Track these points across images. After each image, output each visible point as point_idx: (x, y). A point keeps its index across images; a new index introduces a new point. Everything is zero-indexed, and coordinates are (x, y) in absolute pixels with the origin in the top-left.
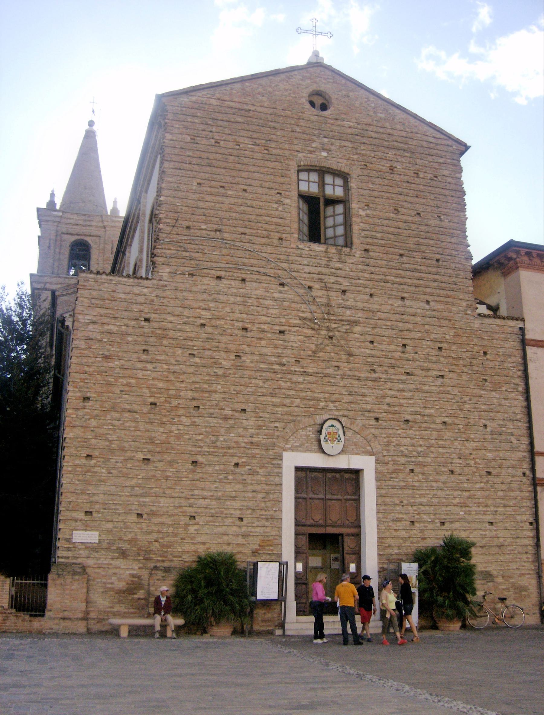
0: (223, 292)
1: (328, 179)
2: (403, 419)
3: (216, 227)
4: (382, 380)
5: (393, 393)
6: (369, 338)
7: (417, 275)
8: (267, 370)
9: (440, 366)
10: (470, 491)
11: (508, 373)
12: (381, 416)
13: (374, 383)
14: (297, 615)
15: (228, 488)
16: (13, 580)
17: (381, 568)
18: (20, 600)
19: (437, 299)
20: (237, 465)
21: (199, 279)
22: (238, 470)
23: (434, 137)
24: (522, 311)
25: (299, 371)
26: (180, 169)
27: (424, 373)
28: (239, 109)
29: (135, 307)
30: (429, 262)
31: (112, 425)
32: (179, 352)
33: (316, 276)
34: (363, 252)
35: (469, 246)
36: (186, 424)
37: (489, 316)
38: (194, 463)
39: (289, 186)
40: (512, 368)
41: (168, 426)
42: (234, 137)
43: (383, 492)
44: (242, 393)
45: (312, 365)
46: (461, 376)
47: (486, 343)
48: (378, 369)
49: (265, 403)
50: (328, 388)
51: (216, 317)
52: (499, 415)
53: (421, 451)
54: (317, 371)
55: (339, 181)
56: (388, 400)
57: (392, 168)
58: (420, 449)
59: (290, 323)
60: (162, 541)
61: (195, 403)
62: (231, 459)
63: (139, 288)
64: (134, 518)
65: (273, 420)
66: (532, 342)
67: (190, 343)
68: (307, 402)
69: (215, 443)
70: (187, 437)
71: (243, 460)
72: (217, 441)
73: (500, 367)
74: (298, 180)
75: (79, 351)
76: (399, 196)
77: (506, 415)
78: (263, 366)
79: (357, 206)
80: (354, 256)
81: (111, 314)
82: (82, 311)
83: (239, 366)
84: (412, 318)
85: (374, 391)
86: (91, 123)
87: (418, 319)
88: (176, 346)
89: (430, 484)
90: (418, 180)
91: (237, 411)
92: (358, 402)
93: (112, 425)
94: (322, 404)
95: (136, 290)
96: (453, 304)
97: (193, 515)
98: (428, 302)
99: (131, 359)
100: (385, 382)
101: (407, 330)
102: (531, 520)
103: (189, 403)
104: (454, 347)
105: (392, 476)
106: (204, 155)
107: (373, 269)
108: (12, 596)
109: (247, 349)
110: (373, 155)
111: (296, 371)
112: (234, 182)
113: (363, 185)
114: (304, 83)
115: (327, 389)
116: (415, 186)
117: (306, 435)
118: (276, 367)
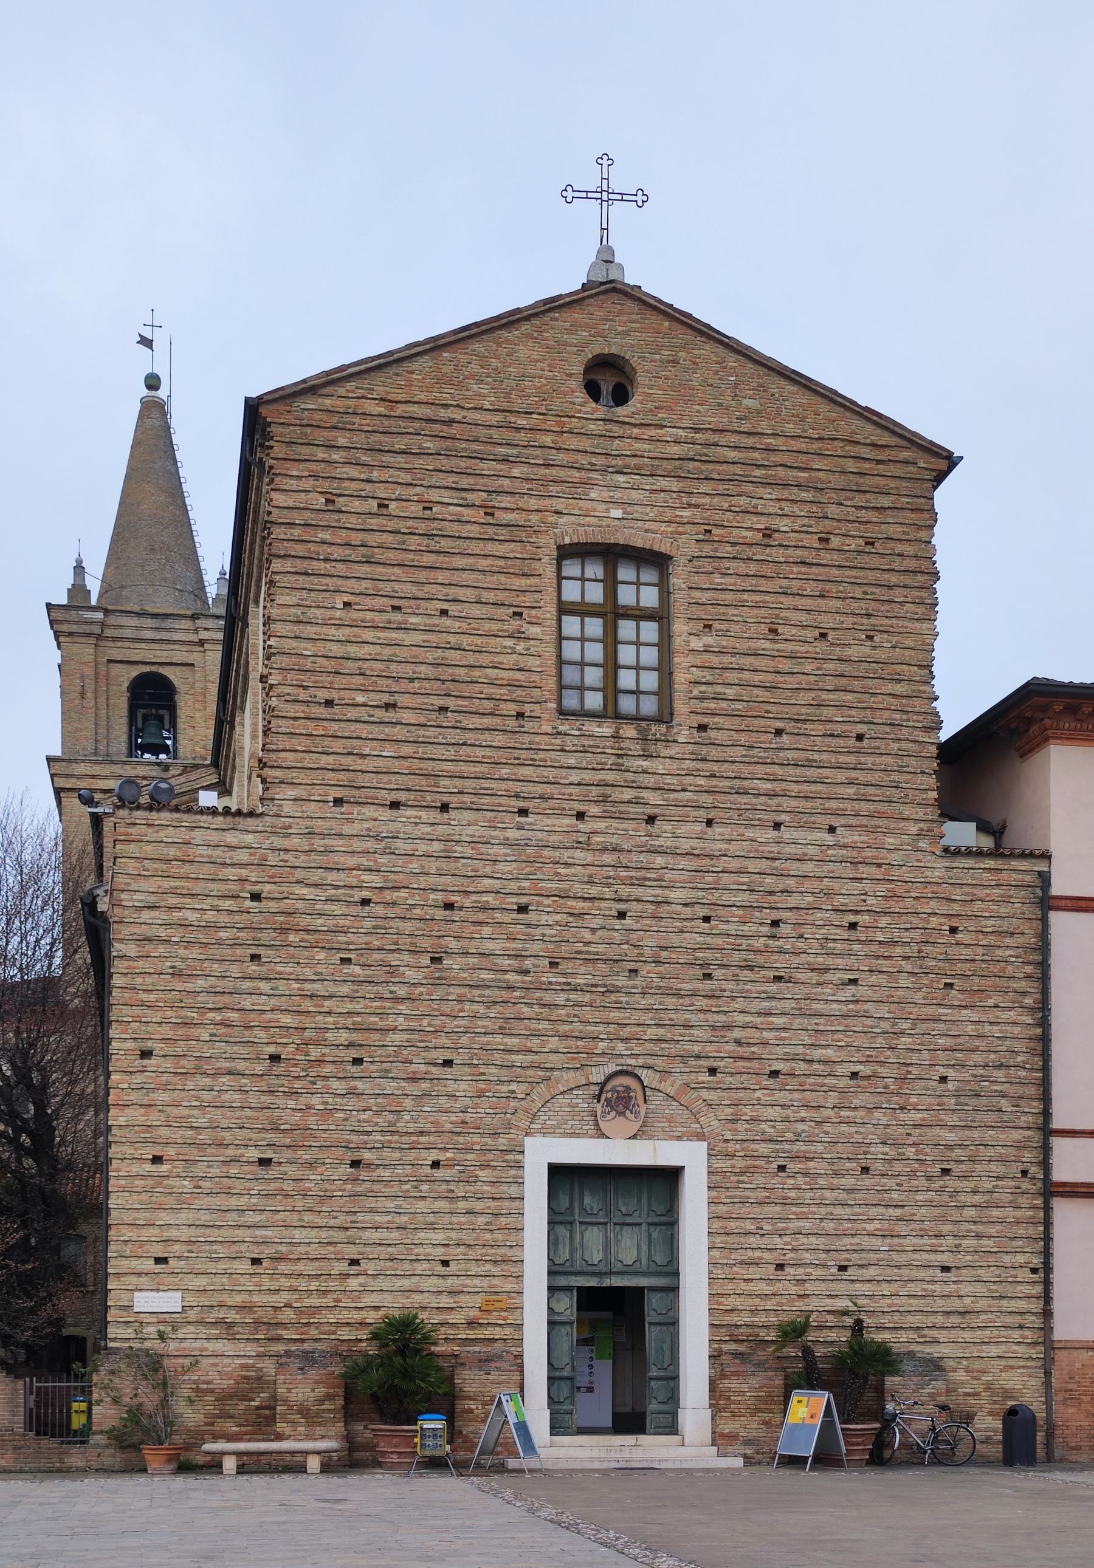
0: (404, 833)
1: (625, 573)
2: (767, 1071)
3: (386, 698)
4: (725, 994)
5: (748, 1018)
6: (702, 912)
7: (811, 773)
8: (494, 984)
9: (851, 962)
10: (904, 1206)
11: (1004, 970)
12: (722, 1064)
13: (710, 1002)
14: (552, 1434)
15: (421, 1206)
16: (31, 1381)
17: (716, 1350)
18: (46, 1415)
19: (854, 821)
20: (436, 1164)
21: (356, 809)
22: (439, 1174)
23: (874, 445)
24: (1047, 837)
25: (557, 983)
26: (307, 574)
27: (815, 977)
28: (429, 420)
29: (231, 873)
30: (841, 742)
31: (198, 1098)
32: (322, 955)
33: (595, 791)
34: (695, 731)
35: (936, 699)
36: (338, 1092)
37: (980, 854)
38: (355, 1164)
39: (538, 596)
40: (1013, 959)
41: (304, 1100)
42: (418, 489)
43: (722, 1209)
44: (446, 1030)
45: (583, 970)
46: (896, 980)
47: (956, 908)
48: (718, 973)
49: (489, 1047)
50: (614, 1015)
51: (391, 885)
52: (977, 1058)
53: (804, 1131)
54: (594, 982)
55: (649, 575)
56: (737, 1034)
57: (768, 532)
58: (800, 1127)
59: (542, 888)
60: (299, 1305)
61: (355, 1053)
62: (424, 1154)
63: (237, 833)
64: (246, 1266)
65: (506, 1079)
66: (1064, 903)
67: (342, 938)
68: (571, 1042)
69: (394, 1125)
70: (341, 1115)
71: (449, 1155)
72: (397, 1121)
73: (986, 958)
74: (560, 578)
75: (126, 964)
76: (782, 598)
77: (993, 1056)
78: (485, 976)
79: (686, 628)
80: (675, 741)
81: (183, 888)
82: (126, 884)
83: (439, 978)
84: (797, 864)
85: (709, 1016)
86: (153, 382)
87: (808, 867)
88: (315, 945)
89: (819, 1193)
90: (826, 557)
91: (435, 1064)
92: (676, 1038)
93: (198, 1098)
94: (602, 1045)
95: (231, 838)
96: (889, 832)
97: (355, 1257)
98: (832, 830)
99: (228, 974)
100: (733, 998)
101: (782, 892)
102: (1036, 1261)
103: (342, 1053)
104: (884, 921)
105: (741, 1178)
106: (356, 538)
107: (715, 767)
108: (31, 1410)
109: (454, 945)
110: (726, 505)
111: (550, 983)
112: (420, 595)
113: (702, 581)
114: (573, 339)
115: (612, 1014)
116: (821, 569)
117: (569, 1105)
118: (512, 977)
